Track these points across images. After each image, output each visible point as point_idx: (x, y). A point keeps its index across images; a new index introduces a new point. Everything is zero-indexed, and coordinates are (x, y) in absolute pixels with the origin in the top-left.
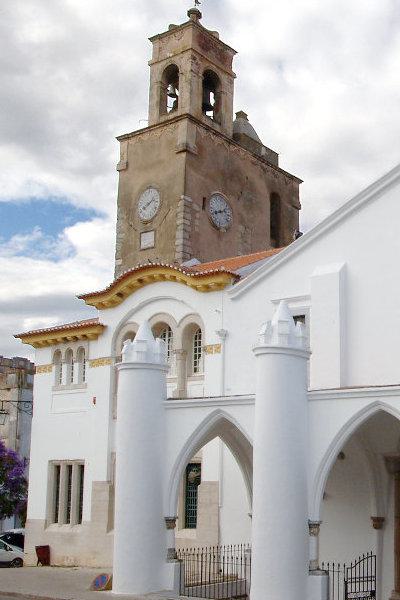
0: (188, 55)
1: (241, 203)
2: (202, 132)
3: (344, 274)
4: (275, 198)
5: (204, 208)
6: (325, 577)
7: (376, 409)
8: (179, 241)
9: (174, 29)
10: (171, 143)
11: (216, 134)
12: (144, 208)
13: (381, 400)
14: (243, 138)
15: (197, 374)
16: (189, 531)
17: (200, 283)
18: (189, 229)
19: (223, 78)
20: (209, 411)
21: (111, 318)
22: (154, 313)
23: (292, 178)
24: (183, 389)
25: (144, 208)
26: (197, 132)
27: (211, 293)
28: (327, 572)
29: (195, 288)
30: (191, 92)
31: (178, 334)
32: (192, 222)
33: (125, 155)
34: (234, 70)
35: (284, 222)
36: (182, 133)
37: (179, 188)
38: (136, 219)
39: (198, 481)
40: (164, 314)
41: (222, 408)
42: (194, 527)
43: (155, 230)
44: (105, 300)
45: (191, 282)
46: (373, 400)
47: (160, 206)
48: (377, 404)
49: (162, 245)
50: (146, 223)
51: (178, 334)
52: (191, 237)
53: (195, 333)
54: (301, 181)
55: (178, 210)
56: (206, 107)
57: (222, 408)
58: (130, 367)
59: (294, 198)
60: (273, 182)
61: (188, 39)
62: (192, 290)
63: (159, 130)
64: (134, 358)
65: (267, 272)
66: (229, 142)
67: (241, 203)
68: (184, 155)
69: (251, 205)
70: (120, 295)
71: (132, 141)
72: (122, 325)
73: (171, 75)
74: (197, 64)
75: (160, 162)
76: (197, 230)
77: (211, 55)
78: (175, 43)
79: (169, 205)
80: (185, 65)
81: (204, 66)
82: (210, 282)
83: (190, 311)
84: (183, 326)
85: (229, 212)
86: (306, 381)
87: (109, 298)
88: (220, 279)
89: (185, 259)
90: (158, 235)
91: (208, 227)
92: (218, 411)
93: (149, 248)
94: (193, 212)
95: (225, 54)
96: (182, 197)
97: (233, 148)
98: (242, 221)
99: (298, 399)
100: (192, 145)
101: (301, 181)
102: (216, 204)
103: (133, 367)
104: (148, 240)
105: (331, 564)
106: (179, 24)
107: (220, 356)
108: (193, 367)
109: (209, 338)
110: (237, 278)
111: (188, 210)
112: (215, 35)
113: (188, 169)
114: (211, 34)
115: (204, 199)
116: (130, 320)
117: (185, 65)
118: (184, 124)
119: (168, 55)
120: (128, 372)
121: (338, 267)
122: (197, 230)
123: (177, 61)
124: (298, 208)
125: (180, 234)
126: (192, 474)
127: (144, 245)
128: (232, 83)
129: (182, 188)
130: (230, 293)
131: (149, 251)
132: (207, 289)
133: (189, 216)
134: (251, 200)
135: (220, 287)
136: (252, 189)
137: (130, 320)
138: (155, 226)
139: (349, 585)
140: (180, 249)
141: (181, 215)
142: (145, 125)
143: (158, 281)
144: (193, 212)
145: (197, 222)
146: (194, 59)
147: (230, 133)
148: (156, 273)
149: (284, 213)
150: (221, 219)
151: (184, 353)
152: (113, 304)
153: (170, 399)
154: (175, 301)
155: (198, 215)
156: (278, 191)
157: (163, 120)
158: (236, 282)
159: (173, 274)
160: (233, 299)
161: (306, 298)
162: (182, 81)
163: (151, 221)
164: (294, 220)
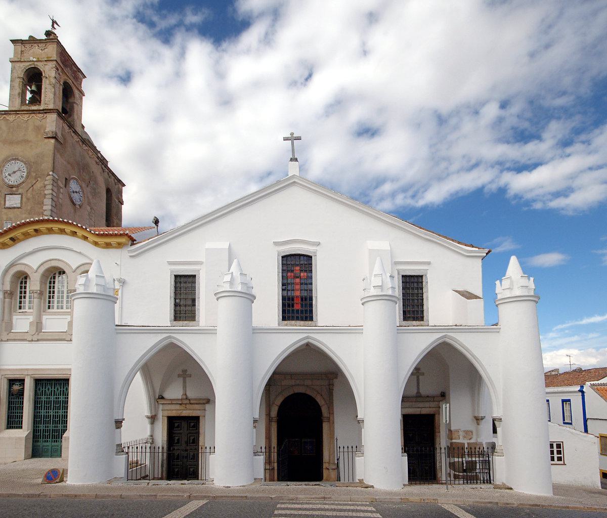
1: (89, 189)
2: (66, 128)
4: (108, 191)
6: (127, 455)
9: (32, 40)
10: (38, 129)
12: (9, 175)
15: (49, 310)
18: (55, 199)
19: (76, 92)
20: (160, 337)
22: (51, 258)
23: (119, 181)
24: (38, 325)
26: (63, 126)
27: (111, 250)
28: (127, 453)
30: (55, 94)
35: (114, 211)
37: (47, 165)
43: (21, 194)
45: (91, 238)
46: (306, 335)
47: (27, 177)
48: (169, 337)
49: (29, 208)
50: (12, 187)
58: (92, 296)
59: (120, 197)
60: (107, 179)
67: (89, 189)
68: (53, 141)
69: (95, 193)
70: (12, 239)
74: (59, 74)
75: (27, 141)
79: (36, 178)
81: (64, 78)
88: (123, 240)
90: (24, 199)
91: (69, 203)
93: (14, 208)
94: (59, 188)
96: (51, 173)
98: (89, 204)
102: (74, 186)
103: (90, 296)
105: (354, 447)
106: (38, 38)
108: (47, 305)
111: (55, 184)
113: (56, 153)
116: (24, 261)
117: (49, 72)
119: (31, 59)
120: (87, 300)
121: (226, 245)
123: (40, 66)
124: (122, 203)
126: (16, 387)
127: (8, 204)
129: (50, 165)
131: (17, 211)
132: (108, 246)
133: (55, 190)
134: (94, 189)
135: (120, 246)
136: (96, 183)
137: (24, 261)
138: (20, 191)
141: (50, 187)
144: (59, 188)
145: (61, 196)
146: (57, 69)
149: (113, 205)
150: (76, 197)
153: (117, 326)
155: (61, 190)
158: (132, 244)
159: (74, 229)
160: (131, 256)
163: (17, 186)
164: (119, 211)
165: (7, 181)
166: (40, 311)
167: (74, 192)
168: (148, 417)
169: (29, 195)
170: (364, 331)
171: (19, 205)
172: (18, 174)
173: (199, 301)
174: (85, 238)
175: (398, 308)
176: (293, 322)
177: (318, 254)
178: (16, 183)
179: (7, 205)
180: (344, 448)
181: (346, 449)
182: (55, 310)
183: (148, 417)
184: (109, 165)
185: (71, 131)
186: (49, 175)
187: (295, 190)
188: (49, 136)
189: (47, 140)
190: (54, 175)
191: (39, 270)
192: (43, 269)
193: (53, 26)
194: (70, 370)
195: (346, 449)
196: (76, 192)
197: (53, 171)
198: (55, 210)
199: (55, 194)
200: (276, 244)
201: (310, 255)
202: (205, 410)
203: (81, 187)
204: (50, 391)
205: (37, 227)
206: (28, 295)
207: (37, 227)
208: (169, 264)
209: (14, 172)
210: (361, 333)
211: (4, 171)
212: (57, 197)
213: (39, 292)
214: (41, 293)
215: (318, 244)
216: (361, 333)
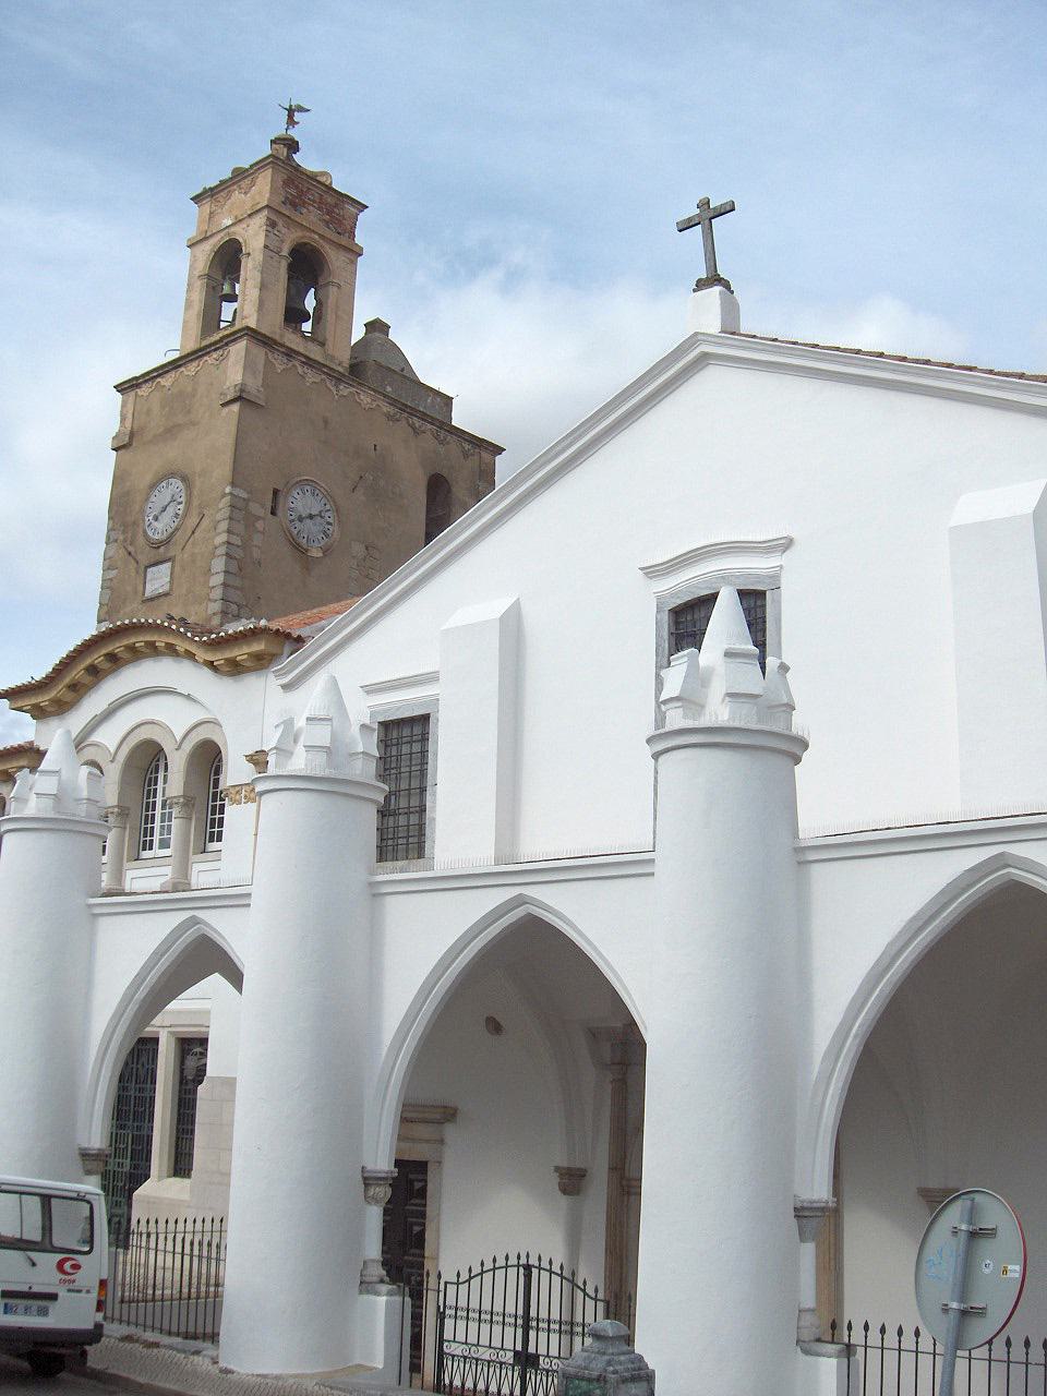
0: (260, 221)
2: (280, 364)
3: (512, 628)
5: (273, 513)
7: (519, 913)
8: (217, 580)
9: (239, 175)
11: (310, 362)
13: (530, 891)
14: (377, 367)
16: (177, 1180)
17: (218, 657)
18: (239, 553)
19: (335, 258)
21: (54, 738)
22: (138, 720)
24: (181, 884)
25: (156, 519)
26: (268, 362)
29: (211, 665)
31: (177, 762)
32: (245, 546)
33: (130, 416)
34: (360, 238)
36: (233, 368)
38: (141, 540)
39: (201, 1073)
40: (152, 723)
41: (200, 914)
42: (189, 1176)
44: (43, 699)
45: (202, 655)
47: (185, 515)
48: (520, 901)
50: (157, 545)
51: (177, 762)
52: (241, 567)
53: (208, 758)
54: (499, 450)
55: (219, 516)
56: (294, 315)
57: (200, 914)
61: (263, 188)
62: (207, 671)
63: (195, 364)
64: (32, 807)
65: (354, 625)
66: (338, 379)
68: (235, 407)
71: (144, 391)
72: (80, 743)
73: (228, 260)
76: (256, 553)
77: (311, 217)
78: (240, 200)
80: (254, 237)
81: (291, 237)
82: (241, 652)
83: (203, 716)
84: (188, 746)
85: (330, 516)
86: (795, 835)
87: (52, 694)
88: (258, 646)
89: (226, 615)
90: (177, 569)
92: (194, 921)
93: (159, 596)
94: (251, 521)
95: (340, 211)
97: (345, 390)
99: (783, 867)
100: (255, 385)
101: (499, 450)
102: (301, 502)
104: (158, 580)
107: (255, 805)
109: (236, 771)
110: (300, 640)
112: (323, 179)
114: (312, 177)
115: (276, 492)
116: (95, 738)
117: (254, 237)
118: (239, 349)
121: (501, 605)
122: (256, 553)
123: (239, 232)
125: (219, 565)
128: (354, 263)
130: (278, 674)
132: (235, 669)
133: (240, 528)
135: (261, 662)
138: (174, 551)
139: (449, 1323)
140: (217, 593)
141: (224, 526)
142: (176, 355)
143: (163, 654)
145: (257, 539)
147: (345, 357)
148: (139, 640)
151: (188, 802)
152: (61, 708)
154: (174, 699)
155: (259, 525)
156: (445, 473)
157: (211, 339)
161: (430, 678)
162: (250, 269)
163: (167, 541)
165: (150, 533)
166: (122, 859)
167: (301, 519)
168: (557, 1169)
169: (186, 556)
170: (656, 869)
171: (166, 588)
172: (171, 510)
173: (434, 794)
174: (190, 656)
175: (367, 821)
176: (400, 863)
177: (786, 583)
178: (164, 537)
179: (148, 594)
180: (883, 1331)
181: (891, 1339)
182: (157, 851)
183: (557, 1169)
184: (459, 419)
185: (297, 363)
186: (224, 495)
187: (712, 377)
188: (229, 398)
189: (226, 409)
190: (237, 492)
191: (117, 758)
192: (126, 750)
193: (291, 122)
194: (208, 1012)
195: (891, 1339)
196: (311, 517)
197: (233, 484)
198: (237, 582)
199: (236, 540)
200: (652, 572)
201: (760, 587)
202: (442, 1141)
203: (329, 496)
204: (140, 1062)
205: (109, 649)
206: (158, 812)
207: (109, 649)
208: (368, 693)
209: (164, 509)
210: (244, 906)
211: (149, 511)
212: (245, 546)
213: (182, 800)
214: (123, 812)
215: (786, 544)
216: (244, 906)
